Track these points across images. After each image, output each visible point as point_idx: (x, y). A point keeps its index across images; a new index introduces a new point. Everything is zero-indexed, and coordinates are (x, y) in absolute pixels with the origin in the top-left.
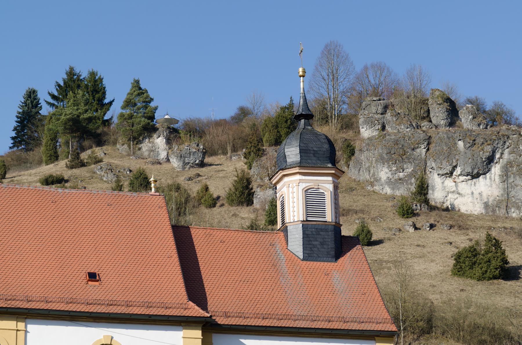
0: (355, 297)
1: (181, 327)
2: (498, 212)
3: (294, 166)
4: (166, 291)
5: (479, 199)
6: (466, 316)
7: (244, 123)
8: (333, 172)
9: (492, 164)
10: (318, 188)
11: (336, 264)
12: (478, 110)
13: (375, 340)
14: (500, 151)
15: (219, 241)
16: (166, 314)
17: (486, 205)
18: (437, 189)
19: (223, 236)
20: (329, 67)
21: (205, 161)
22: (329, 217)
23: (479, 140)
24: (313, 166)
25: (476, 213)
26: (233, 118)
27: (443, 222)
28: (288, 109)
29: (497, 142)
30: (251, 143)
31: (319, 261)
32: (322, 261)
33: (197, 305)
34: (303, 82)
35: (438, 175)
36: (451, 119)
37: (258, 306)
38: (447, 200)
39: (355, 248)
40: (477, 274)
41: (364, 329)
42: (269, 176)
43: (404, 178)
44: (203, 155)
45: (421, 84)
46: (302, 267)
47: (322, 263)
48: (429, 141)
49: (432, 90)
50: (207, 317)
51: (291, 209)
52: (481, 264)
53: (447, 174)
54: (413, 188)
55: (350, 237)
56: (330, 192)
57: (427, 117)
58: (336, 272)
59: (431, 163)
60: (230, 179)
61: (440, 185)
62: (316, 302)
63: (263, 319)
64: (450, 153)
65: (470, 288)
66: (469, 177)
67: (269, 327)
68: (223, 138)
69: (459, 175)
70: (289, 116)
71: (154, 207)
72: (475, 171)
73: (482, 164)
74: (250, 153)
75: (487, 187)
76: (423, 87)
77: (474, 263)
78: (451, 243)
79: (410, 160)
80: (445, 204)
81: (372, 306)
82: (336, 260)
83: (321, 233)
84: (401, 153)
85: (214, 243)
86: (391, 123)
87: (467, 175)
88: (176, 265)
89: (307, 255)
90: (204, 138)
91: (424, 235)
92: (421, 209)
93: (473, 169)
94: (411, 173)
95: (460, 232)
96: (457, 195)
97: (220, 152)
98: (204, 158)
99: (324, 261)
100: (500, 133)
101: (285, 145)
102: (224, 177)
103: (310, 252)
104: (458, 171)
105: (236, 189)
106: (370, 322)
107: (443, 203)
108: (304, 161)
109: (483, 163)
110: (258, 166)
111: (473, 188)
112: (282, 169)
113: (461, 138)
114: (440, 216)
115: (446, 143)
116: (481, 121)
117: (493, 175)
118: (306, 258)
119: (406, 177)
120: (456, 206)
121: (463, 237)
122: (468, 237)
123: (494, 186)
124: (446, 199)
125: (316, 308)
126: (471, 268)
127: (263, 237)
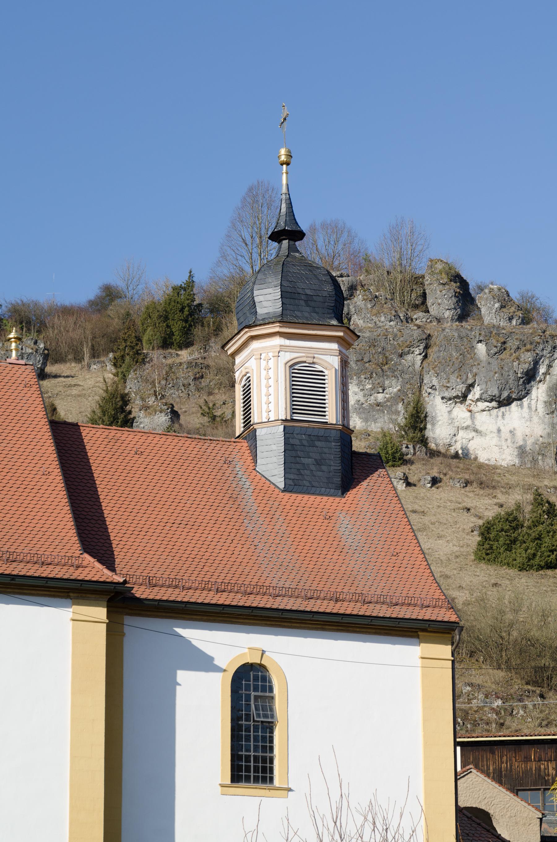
0: (380, 560)
1: (69, 601)
2: (540, 463)
3: (271, 320)
4: (41, 533)
5: (509, 441)
6: (511, 625)
7: (112, 311)
8: (341, 334)
9: (532, 383)
10: (313, 363)
11: (344, 500)
12: (505, 300)
13: (418, 637)
14: (547, 362)
15: (133, 452)
16: (43, 575)
17: (522, 451)
18: (440, 423)
19: (139, 443)
20: (255, 223)
21: (46, 370)
22: (332, 416)
23: (512, 343)
24: (305, 322)
25: (504, 464)
26: (92, 303)
27: (453, 475)
28: (185, 290)
29: (541, 347)
30: (125, 341)
31: (313, 494)
32: (318, 494)
33: (99, 561)
34: (287, 173)
35: (443, 398)
36: (463, 309)
37: (206, 568)
38: (456, 441)
39: (376, 475)
40: (519, 560)
41: (400, 616)
42: (156, 395)
43: (385, 402)
44: (44, 359)
45: (413, 250)
46: (284, 503)
47: (319, 498)
48: (427, 342)
49: (431, 261)
50: (118, 583)
51: (264, 399)
52: (525, 542)
53: (457, 397)
54: (401, 420)
55: (366, 454)
56: (334, 370)
57: (422, 304)
58: (344, 513)
59: (431, 379)
60: (90, 399)
61: (446, 415)
62: (311, 566)
63: (217, 591)
64: (464, 363)
65: (508, 582)
66: (494, 404)
67: (229, 606)
68: (76, 335)
69: (478, 400)
70: (188, 302)
71: (16, 385)
72: (505, 394)
73: (516, 383)
74: (123, 356)
75: (523, 421)
76: (415, 254)
77: (514, 541)
78: (469, 510)
79: (396, 372)
80: (453, 448)
81: (412, 577)
82: (343, 494)
83: (318, 443)
84: (381, 360)
85: (124, 455)
86: (364, 311)
87: (491, 401)
88: (58, 489)
89: (291, 482)
90: (44, 334)
91: (422, 495)
92: (415, 454)
93: (501, 391)
94: (396, 394)
95: (482, 492)
96: (474, 434)
97: (70, 357)
98: (44, 364)
99: (322, 495)
100: (548, 333)
101: (254, 283)
102: (79, 396)
103: (296, 477)
104: (476, 392)
105: (104, 412)
106: (409, 605)
107: (450, 445)
108: (288, 312)
109: (519, 381)
110: (137, 378)
111: (500, 422)
112: (249, 327)
113: (481, 338)
114: (449, 466)
115: (456, 346)
116: (514, 312)
117: (533, 402)
118: (286, 490)
119: (388, 400)
120: (471, 452)
121: (487, 501)
122: (496, 501)
123: (535, 419)
124: (455, 438)
125: (312, 577)
126: (509, 549)
127: (211, 448)
